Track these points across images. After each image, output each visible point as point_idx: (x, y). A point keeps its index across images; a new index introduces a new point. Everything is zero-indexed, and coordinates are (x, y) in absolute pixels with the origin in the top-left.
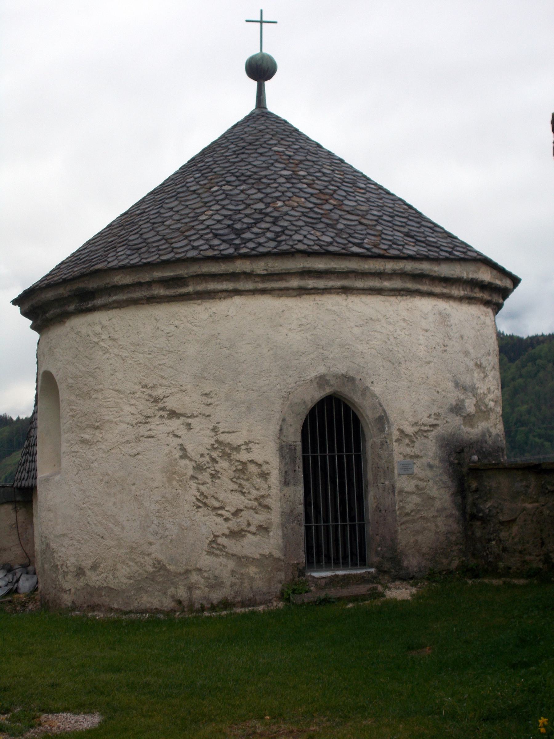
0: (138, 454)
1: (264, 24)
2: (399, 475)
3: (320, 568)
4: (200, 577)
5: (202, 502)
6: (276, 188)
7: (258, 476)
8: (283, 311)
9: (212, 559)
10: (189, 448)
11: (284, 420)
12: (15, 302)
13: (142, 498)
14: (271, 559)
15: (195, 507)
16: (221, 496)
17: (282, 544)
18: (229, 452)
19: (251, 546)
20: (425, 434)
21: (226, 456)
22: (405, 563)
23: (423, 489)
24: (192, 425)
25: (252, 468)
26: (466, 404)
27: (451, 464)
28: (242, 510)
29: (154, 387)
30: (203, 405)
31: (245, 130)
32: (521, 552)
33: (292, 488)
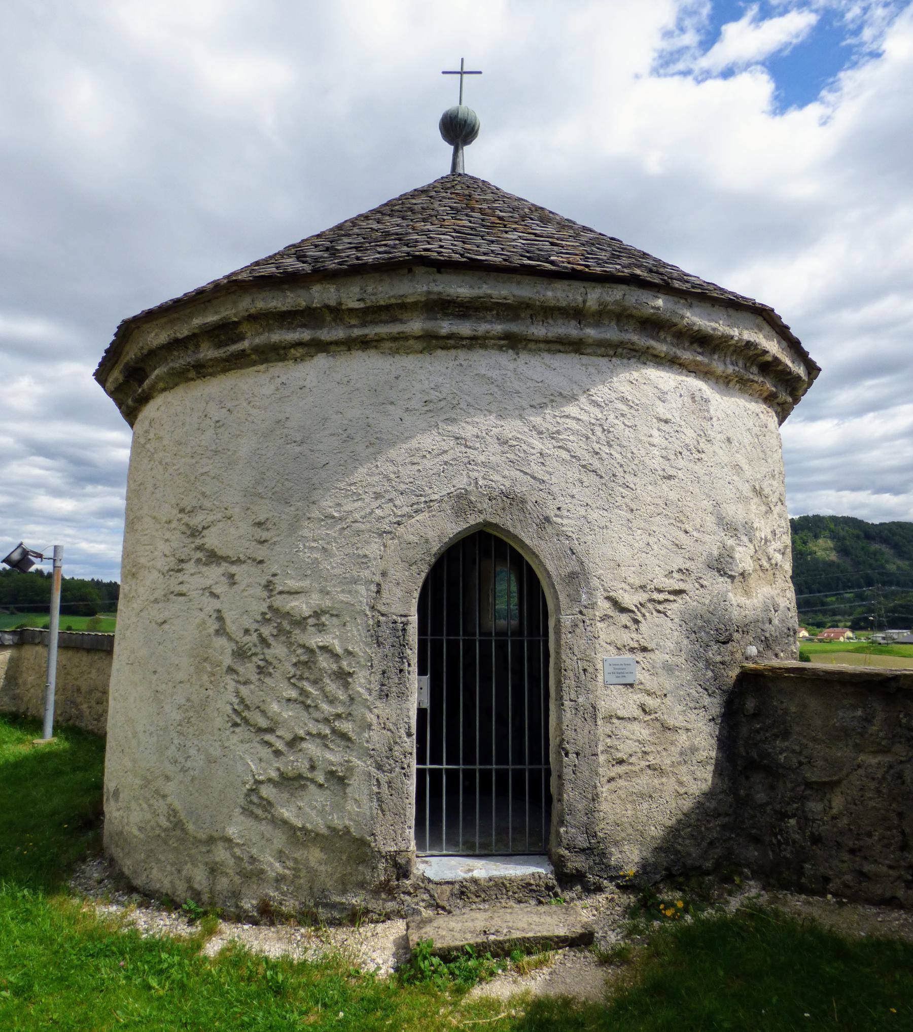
0: (165, 622)
1: (465, 75)
2: (606, 685)
4: (228, 855)
5: (240, 717)
7: (333, 677)
8: (397, 378)
10: (229, 616)
14: (347, 837)
15: (230, 724)
18: (288, 628)
24: (236, 577)
25: (324, 662)
28: (302, 739)
29: (192, 511)
30: (254, 543)
32: (852, 851)
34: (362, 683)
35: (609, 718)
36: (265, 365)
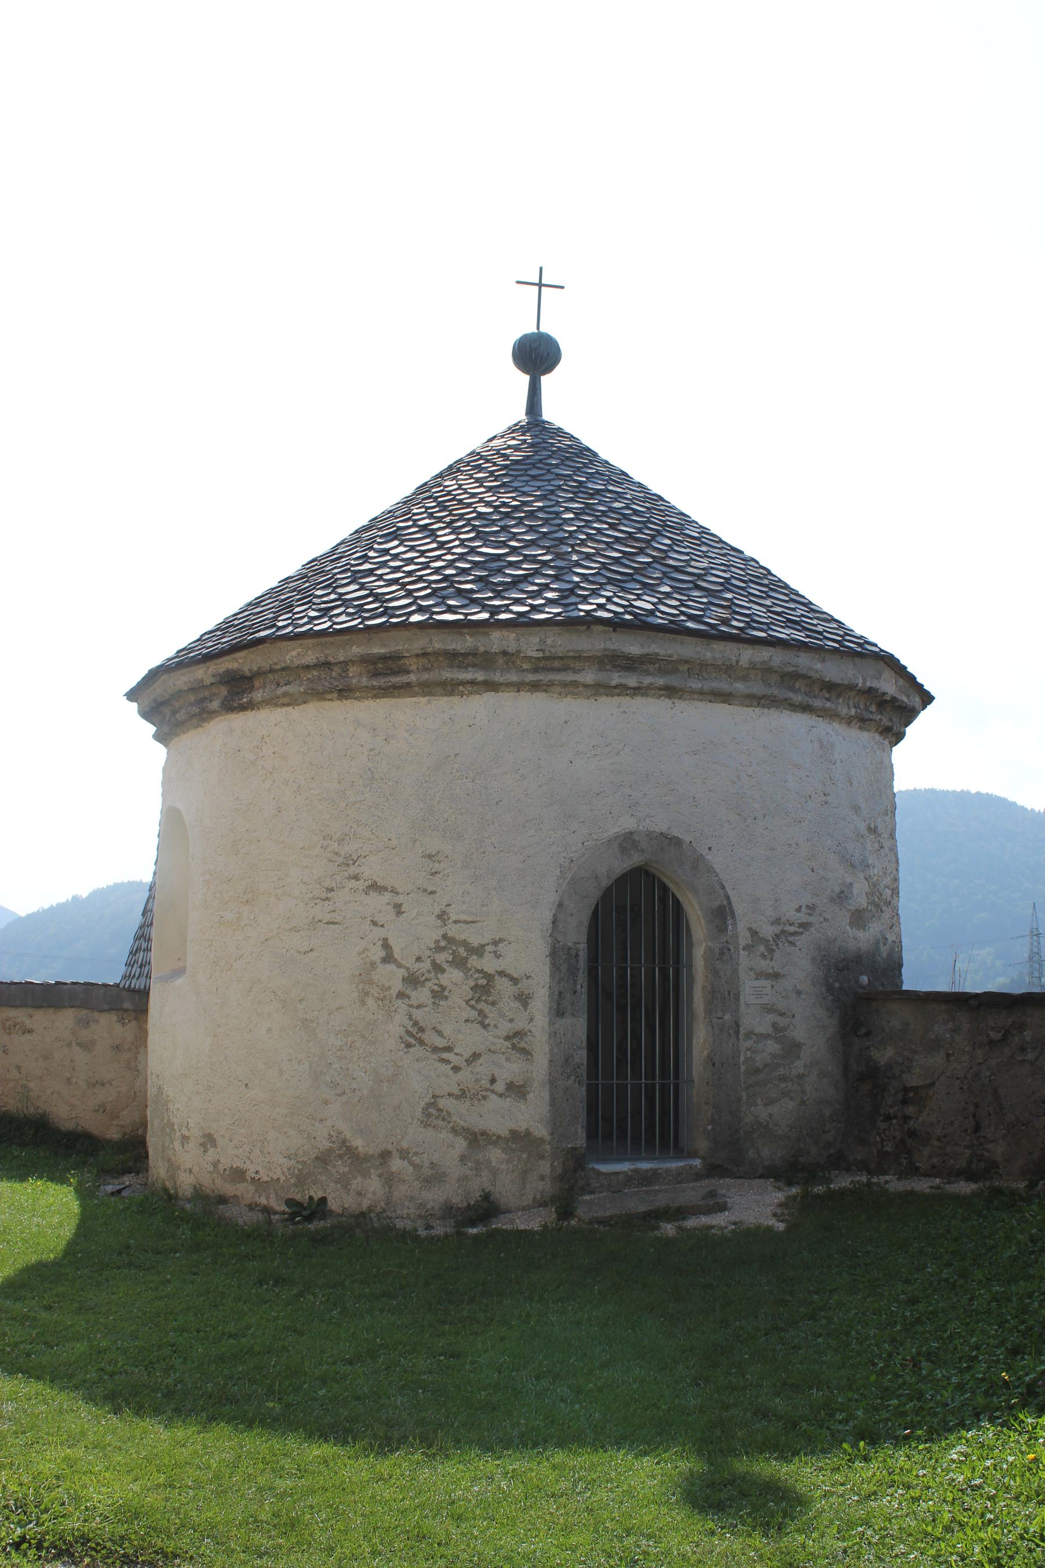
6: (559, 525)
9: (430, 1132)
11: (560, 905)
12: (132, 695)
13: (314, 1025)
16: (447, 1030)
17: (548, 1115)
19: (498, 1116)
20: (791, 939)
21: (459, 963)
22: (751, 1154)
23: (785, 1029)
26: (855, 892)
27: (830, 988)
31: (509, 443)
33: (568, 1020)
35: (749, 1034)
36: (427, 698)
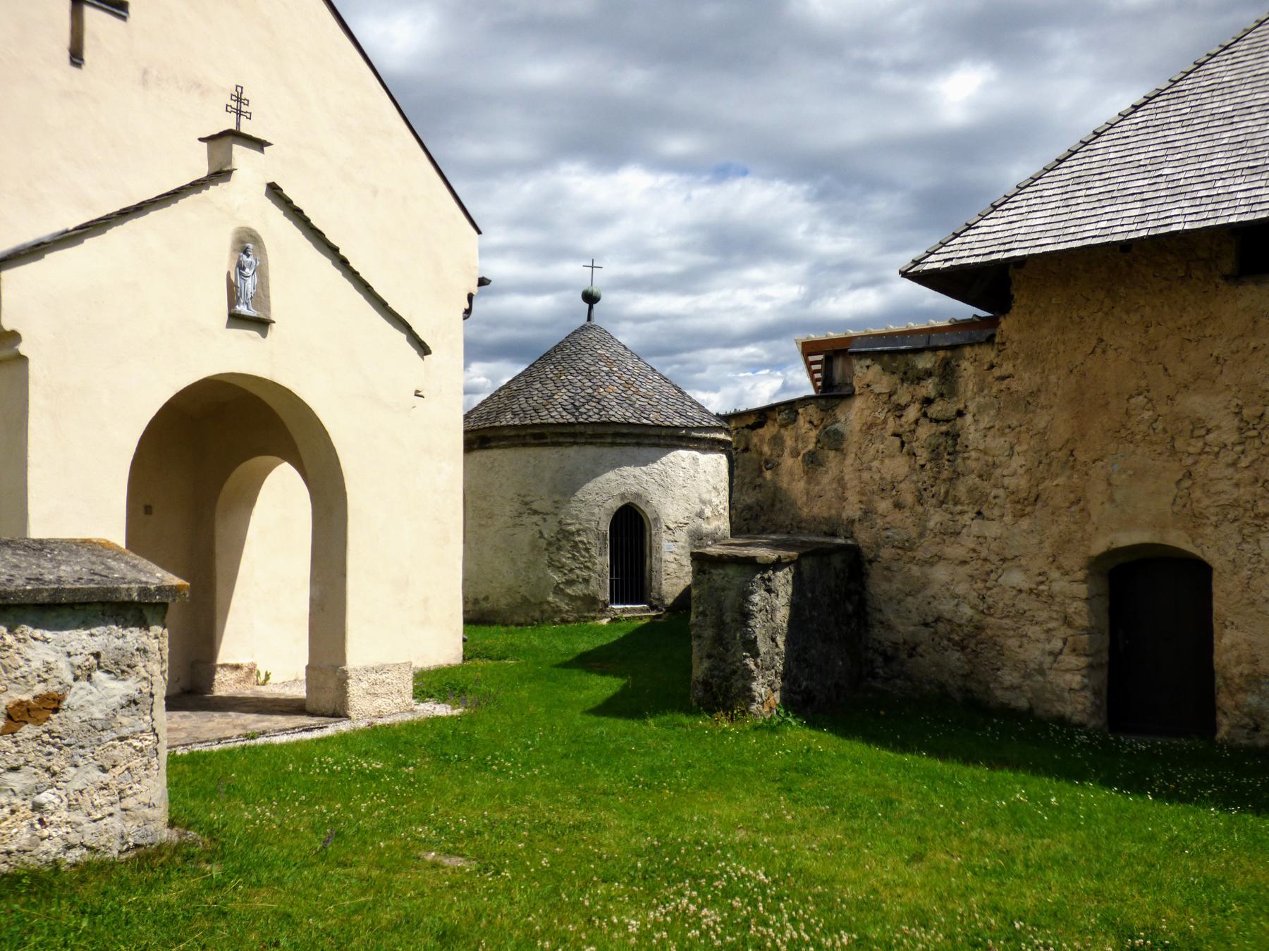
3: (617, 603)
34: (594, 551)
